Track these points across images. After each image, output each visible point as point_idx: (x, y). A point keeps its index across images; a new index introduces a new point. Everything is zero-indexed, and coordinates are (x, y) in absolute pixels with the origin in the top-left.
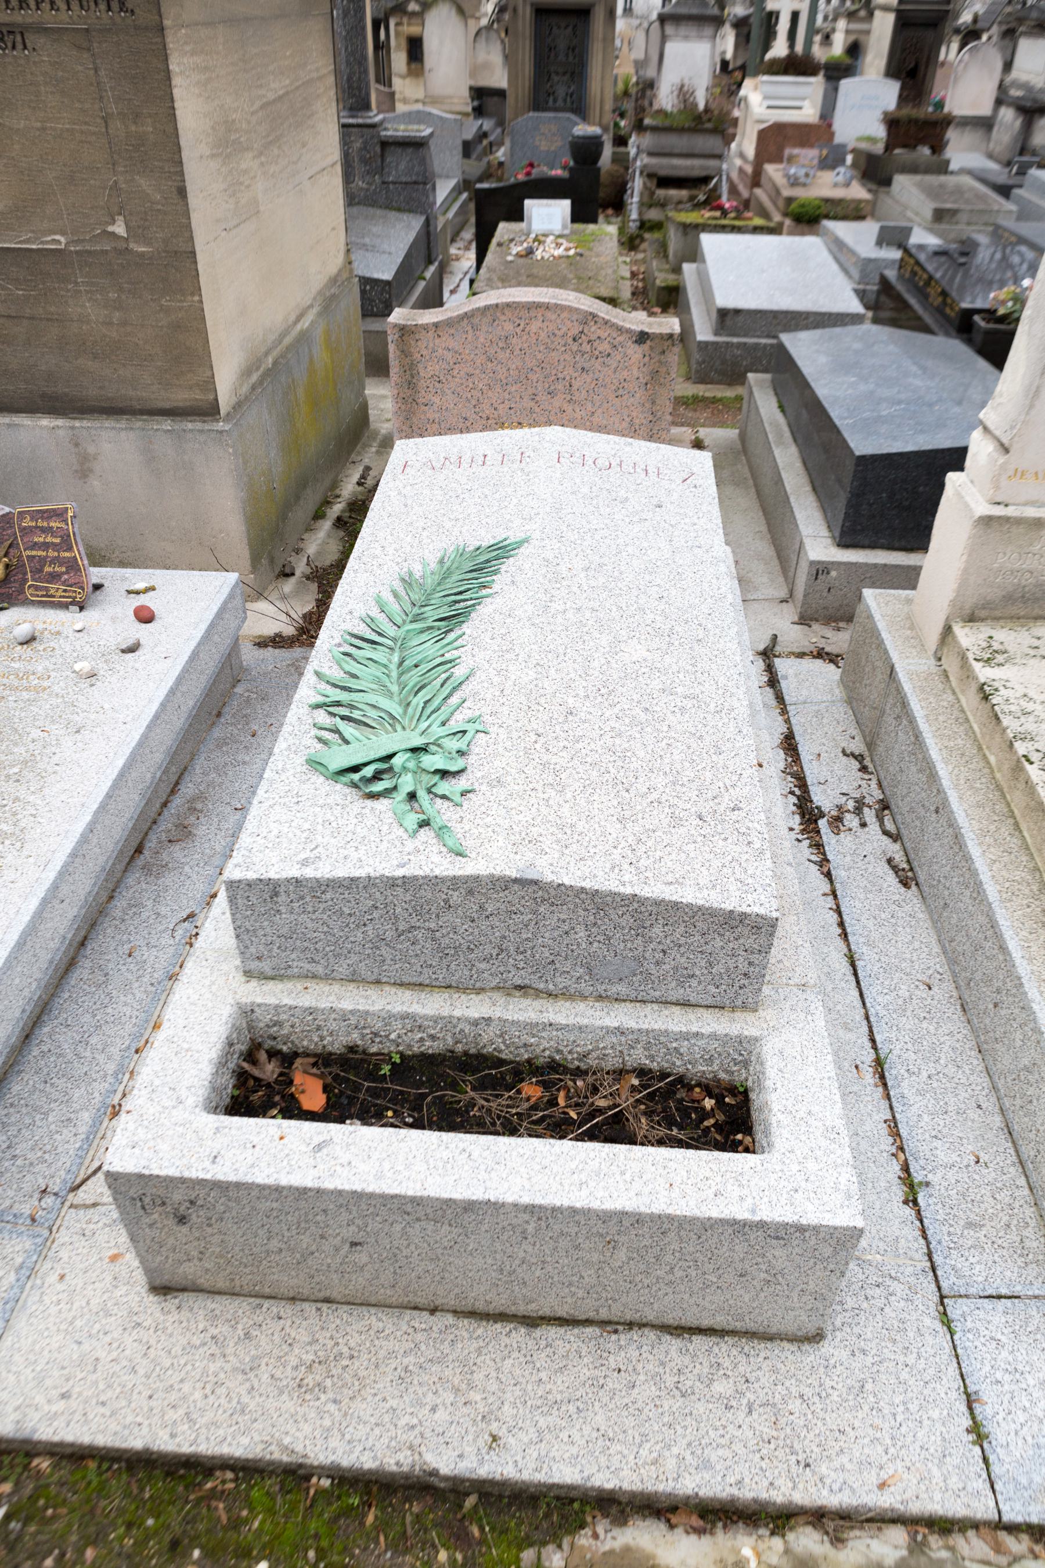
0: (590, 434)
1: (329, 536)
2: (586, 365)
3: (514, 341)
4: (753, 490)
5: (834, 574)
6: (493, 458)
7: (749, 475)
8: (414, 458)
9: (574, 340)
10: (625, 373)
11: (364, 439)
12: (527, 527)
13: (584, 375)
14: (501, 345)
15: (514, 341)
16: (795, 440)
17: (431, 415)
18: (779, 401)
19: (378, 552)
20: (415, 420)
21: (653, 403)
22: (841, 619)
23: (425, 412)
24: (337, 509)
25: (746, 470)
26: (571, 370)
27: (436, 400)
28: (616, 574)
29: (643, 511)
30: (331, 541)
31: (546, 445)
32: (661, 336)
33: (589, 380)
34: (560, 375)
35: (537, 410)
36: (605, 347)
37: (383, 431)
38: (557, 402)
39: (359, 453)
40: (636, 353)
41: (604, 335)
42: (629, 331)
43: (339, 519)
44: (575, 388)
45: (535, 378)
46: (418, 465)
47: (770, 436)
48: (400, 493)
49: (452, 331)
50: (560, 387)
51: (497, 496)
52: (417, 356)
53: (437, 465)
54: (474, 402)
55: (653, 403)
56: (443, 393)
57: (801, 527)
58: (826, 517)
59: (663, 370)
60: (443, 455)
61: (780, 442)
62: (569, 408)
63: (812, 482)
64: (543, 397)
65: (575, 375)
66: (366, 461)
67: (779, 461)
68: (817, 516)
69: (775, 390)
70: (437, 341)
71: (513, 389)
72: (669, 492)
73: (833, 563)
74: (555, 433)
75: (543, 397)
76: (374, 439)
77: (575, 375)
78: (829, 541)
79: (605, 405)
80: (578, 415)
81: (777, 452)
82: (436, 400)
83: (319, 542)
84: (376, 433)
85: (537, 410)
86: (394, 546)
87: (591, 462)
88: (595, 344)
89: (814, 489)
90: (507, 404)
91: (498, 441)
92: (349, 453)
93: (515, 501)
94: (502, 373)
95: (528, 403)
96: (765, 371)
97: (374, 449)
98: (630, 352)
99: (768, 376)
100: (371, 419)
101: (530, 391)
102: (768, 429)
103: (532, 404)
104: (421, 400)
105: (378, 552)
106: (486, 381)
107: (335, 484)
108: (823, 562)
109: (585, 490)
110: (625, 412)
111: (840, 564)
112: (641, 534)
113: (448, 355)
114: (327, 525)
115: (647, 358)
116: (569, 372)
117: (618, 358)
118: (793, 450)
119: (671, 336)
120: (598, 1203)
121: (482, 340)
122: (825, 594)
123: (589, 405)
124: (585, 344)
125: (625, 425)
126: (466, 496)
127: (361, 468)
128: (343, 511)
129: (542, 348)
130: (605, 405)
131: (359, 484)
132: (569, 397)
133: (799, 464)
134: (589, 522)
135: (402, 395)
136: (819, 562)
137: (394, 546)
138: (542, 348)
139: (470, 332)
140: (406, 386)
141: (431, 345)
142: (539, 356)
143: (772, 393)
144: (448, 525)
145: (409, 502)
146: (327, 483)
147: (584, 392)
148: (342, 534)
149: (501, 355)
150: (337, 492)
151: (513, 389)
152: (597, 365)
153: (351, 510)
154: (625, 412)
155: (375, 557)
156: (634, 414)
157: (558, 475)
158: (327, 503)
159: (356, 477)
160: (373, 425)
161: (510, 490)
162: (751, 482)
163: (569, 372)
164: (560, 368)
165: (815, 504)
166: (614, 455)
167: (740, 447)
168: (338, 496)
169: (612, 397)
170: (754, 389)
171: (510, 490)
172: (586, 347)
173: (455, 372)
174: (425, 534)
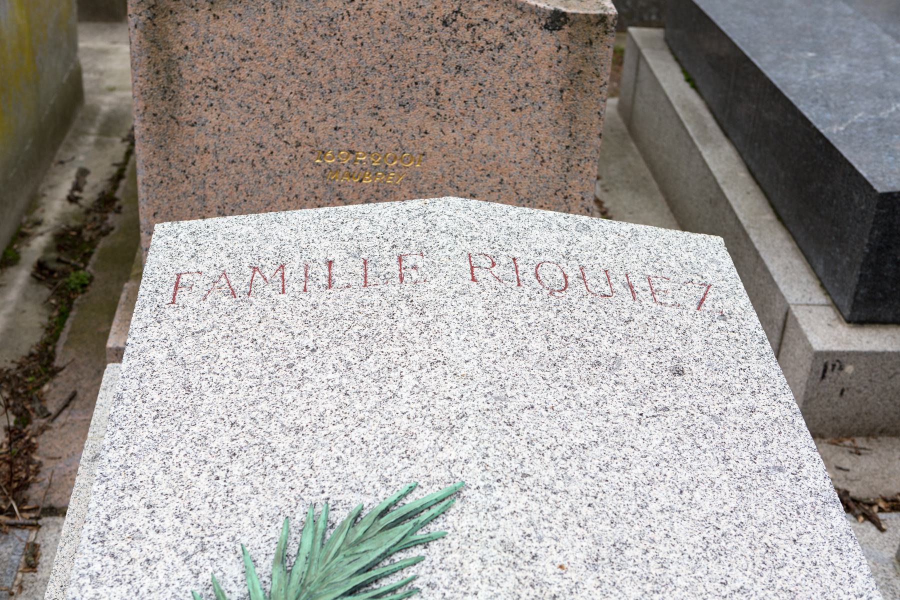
0: (515, 211)
1: (25, 297)
2: (463, 62)
3: (344, 25)
4: (661, 198)
5: (849, 369)
6: (347, 270)
7: (647, 172)
8: (192, 266)
9: (445, 23)
10: (528, 74)
11: (76, 123)
12: (450, 453)
13: (461, 77)
14: (321, 31)
15: (344, 25)
16: (726, 135)
17: (201, 140)
18: (684, 71)
19: (140, 521)
20: (173, 148)
21: (573, 119)
22: (859, 434)
23: (190, 136)
24: (37, 246)
25: (642, 165)
26: (439, 71)
27: (211, 117)
28: (654, 568)
29: (653, 386)
30: (29, 306)
31: (443, 240)
32: (587, 19)
33: (468, 85)
34: (420, 78)
35: (381, 130)
36: (496, 34)
37: (105, 109)
38: (415, 119)
39: (70, 147)
40: (545, 43)
41: (493, 16)
42: (535, 10)
43: (41, 266)
44: (445, 96)
45: (378, 81)
46: (201, 283)
47: (689, 128)
48: (172, 357)
49: (239, 9)
50: (420, 95)
51: (370, 365)
52: (178, 48)
53: (240, 285)
54: (274, 120)
55: (573, 119)
56: (223, 106)
57: (782, 288)
58: (813, 268)
59: (589, 69)
60: (247, 260)
61: (707, 140)
62: (434, 128)
63: (772, 205)
64: (390, 111)
65: (444, 77)
66: (81, 160)
67: (713, 169)
68: (798, 264)
69: (673, 53)
70: (213, 25)
71: (342, 99)
72: (684, 333)
73: (848, 354)
74: (452, 214)
75: (390, 111)
76: (92, 121)
77: (444, 77)
78: (830, 313)
79: (494, 123)
80: (449, 138)
81: (706, 154)
82: (211, 117)
83: (9, 309)
84: (94, 111)
85: (381, 130)
86: (175, 503)
87: (530, 276)
88: (479, 30)
89: (779, 217)
90: (331, 123)
91: (348, 230)
92: (54, 149)
93: (409, 380)
94: (322, 73)
95: (365, 120)
96: (658, 26)
97: (91, 139)
98: (535, 42)
99: (658, 33)
100: (87, 87)
101: (370, 102)
102: (682, 116)
103: (372, 122)
104: (185, 117)
105: (140, 521)
106: (295, 88)
107: (34, 203)
108: (834, 353)
109: (537, 345)
110: (527, 133)
111: (858, 354)
112: (667, 448)
113: (232, 47)
114: (21, 275)
115: (563, 53)
116: (435, 72)
117: (517, 51)
118: (727, 149)
119: (602, 19)
120: (146, 279)
121: (290, 23)
122: (835, 398)
123: (468, 122)
124: (463, 29)
125: (526, 152)
126: (308, 364)
127: (73, 172)
128: (47, 250)
129: (390, 36)
130: (494, 123)
131: (72, 199)
132: (434, 111)
133: (743, 175)
134: (566, 429)
135: (151, 110)
136: (828, 353)
137: (175, 503)
138: (390, 36)
139: (270, 10)
140: (158, 94)
141: (203, 31)
142: (386, 48)
143: (670, 58)
144: (283, 443)
145: (194, 380)
146: (22, 202)
147: (460, 104)
148: (46, 292)
149: (321, 47)
150: (37, 215)
151: (342, 99)
152: (482, 61)
153: (59, 248)
154: (527, 133)
155: (135, 536)
156: (542, 136)
157: (481, 313)
158: (21, 236)
159: (66, 187)
160: (90, 99)
161: (395, 350)
162: (654, 185)
163: (435, 72)
164: (421, 66)
165: (789, 245)
166: (567, 256)
167: (623, 127)
168: (38, 223)
169: (505, 111)
170: (645, 52)
171: (395, 350)
172: (465, 35)
173: (243, 74)
174: (237, 468)
